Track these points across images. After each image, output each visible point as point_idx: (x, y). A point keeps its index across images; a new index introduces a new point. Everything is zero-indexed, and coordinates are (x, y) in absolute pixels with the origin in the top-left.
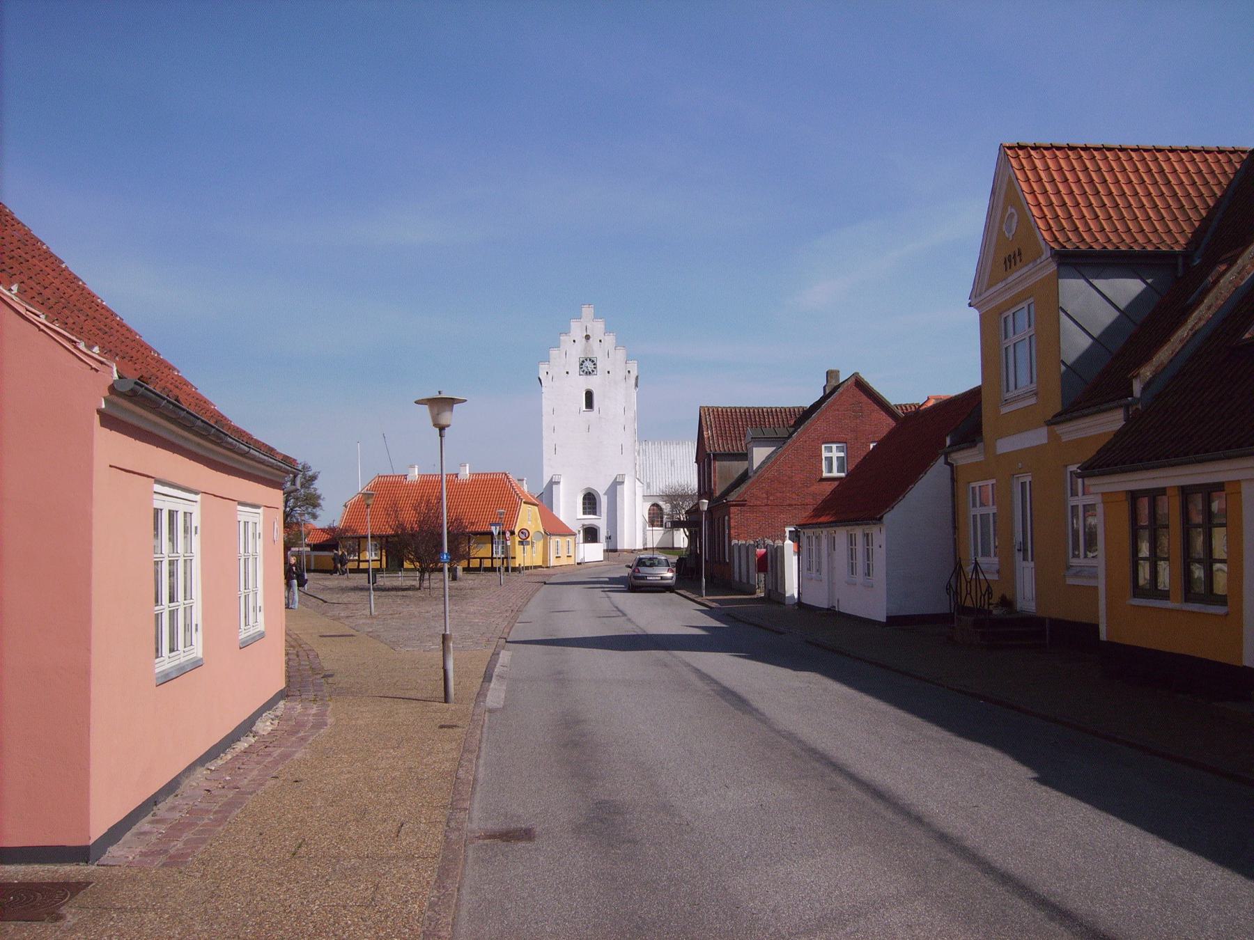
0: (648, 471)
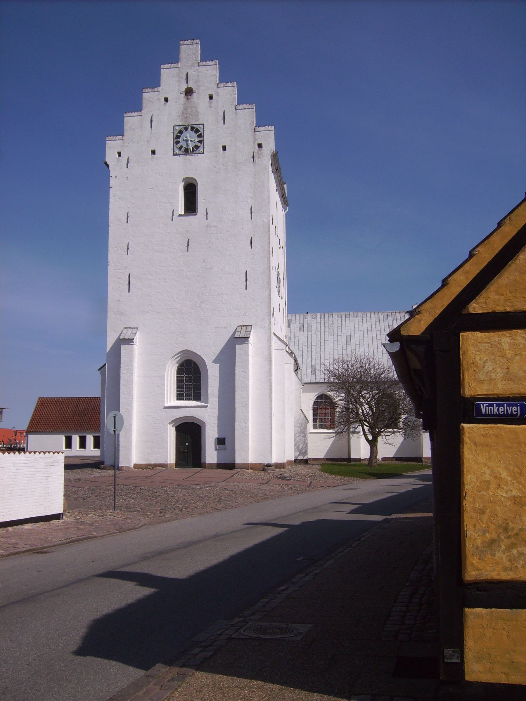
0: (314, 350)
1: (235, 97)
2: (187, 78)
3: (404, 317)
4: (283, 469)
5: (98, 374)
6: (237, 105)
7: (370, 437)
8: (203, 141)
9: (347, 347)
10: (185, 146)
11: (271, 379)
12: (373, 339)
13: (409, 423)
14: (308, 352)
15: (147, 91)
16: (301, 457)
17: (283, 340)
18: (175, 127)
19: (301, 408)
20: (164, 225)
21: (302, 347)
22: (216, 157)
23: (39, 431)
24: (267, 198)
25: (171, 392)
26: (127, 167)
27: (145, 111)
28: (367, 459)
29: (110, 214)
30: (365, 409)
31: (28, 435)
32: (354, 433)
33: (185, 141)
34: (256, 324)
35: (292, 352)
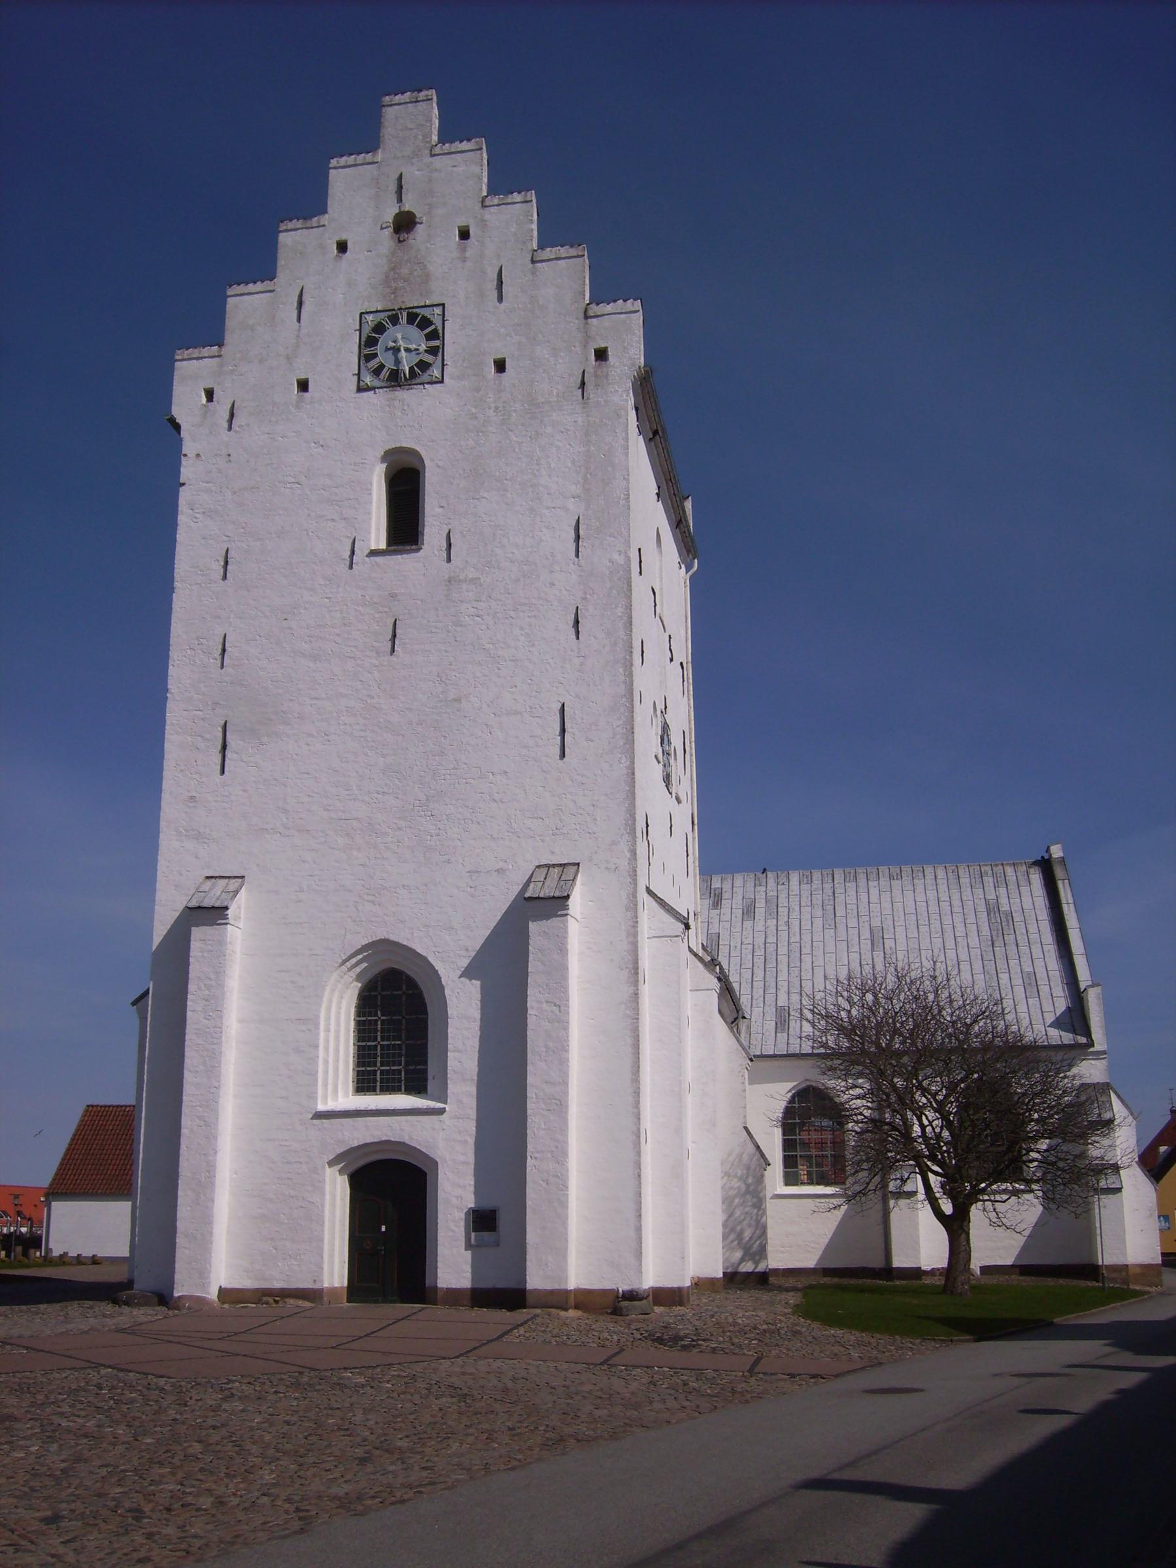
0: (783, 967)
1: (532, 230)
2: (400, 187)
3: (1026, 877)
4: (679, 1308)
5: (131, 1016)
6: (536, 251)
7: (947, 1207)
8: (441, 350)
9: (873, 959)
10: (390, 364)
11: (638, 1027)
12: (946, 935)
13: (1061, 1164)
14: (767, 972)
15: (289, 228)
16: (747, 1267)
17: (686, 916)
18: (363, 316)
19: (745, 1123)
20: (328, 583)
21: (751, 961)
22: (478, 390)
23: (75, 1193)
24: (622, 496)
25: (336, 1069)
26: (230, 428)
27: (282, 276)
28: (938, 1269)
29: (177, 558)
30: (931, 1123)
31: (50, 1203)
32: (900, 1194)
33: (391, 352)
34: (591, 860)
35: (712, 960)
